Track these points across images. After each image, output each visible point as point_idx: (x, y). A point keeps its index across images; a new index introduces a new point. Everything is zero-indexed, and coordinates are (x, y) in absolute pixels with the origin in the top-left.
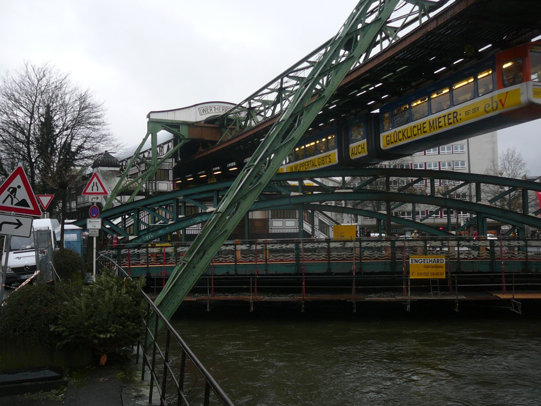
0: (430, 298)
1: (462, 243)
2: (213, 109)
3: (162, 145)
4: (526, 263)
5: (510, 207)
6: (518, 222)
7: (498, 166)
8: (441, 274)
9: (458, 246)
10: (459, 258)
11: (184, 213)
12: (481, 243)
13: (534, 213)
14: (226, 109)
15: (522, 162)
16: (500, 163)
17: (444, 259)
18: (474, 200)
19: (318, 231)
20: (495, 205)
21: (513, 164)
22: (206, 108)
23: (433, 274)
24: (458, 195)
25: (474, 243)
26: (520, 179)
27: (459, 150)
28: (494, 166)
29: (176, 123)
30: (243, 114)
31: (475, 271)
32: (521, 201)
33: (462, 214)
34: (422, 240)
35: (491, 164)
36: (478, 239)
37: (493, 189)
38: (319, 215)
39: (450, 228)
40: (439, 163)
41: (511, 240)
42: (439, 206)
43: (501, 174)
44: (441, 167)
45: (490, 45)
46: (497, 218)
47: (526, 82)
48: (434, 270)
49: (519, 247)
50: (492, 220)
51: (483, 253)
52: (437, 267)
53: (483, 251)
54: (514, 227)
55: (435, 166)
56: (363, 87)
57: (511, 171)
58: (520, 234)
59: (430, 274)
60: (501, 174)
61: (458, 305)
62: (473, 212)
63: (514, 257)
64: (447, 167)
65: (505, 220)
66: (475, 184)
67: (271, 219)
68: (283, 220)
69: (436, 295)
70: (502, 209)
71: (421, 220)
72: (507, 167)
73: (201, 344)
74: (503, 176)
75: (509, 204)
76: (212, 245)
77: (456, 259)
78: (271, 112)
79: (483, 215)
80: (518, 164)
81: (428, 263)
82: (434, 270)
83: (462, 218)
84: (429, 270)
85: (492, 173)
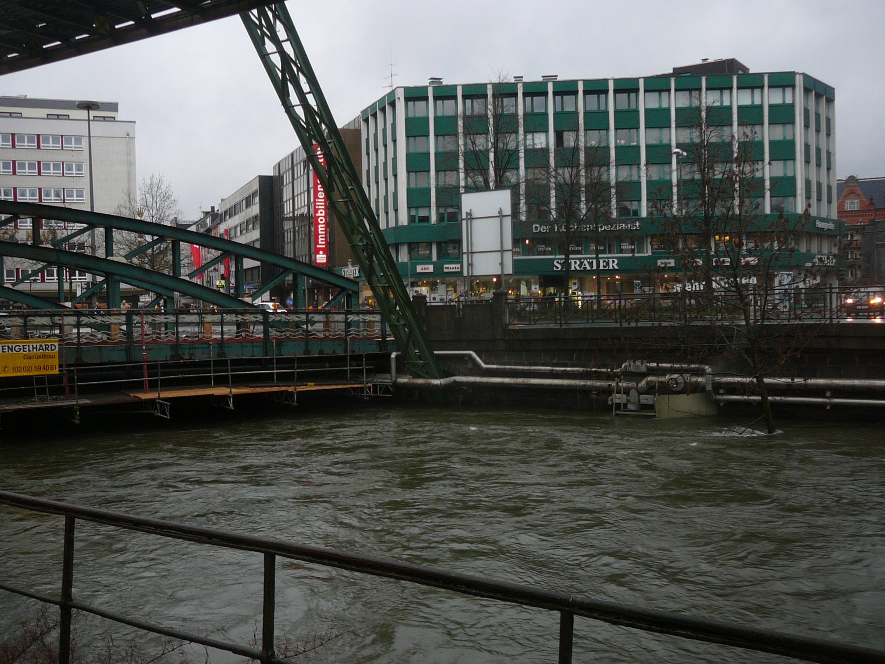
0: (35, 406)
1: (85, 320)
4: (177, 346)
5: (153, 267)
6: (166, 288)
7: (136, 201)
8: (52, 367)
9: (78, 325)
10: (79, 343)
12: (113, 320)
13: (188, 275)
15: (173, 198)
16: (138, 197)
17: (57, 344)
18: (101, 253)
20: (131, 262)
21: (158, 200)
23: (39, 368)
24: (73, 246)
25: (103, 319)
26: (168, 224)
27: (74, 171)
28: (130, 202)
31: (104, 360)
32: (171, 257)
33: (77, 277)
34: (20, 316)
35: (126, 198)
36: (109, 314)
37: (128, 238)
39: (62, 297)
40: (40, 189)
41: (155, 314)
42: (39, 260)
43: (140, 214)
44: (18, 197)
45: (132, 23)
46: (134, 282)
48: (40, 362)
49: (166, 325)
50: (131, 287)
51: (116, 334)
52: (44, 356)
53: (116, 331)
54: (159, 296)
55: (33, 195)
57: (155, 211)
58: (168, 306)
59: (33, 368)
60: (140, 214)
61: (78, 413)
62: (96, 272)
63: (160, 338)
64: (53, 197)
65: (148, 286)
66: (102, 230)
69: (42, 400)
70: (140, 268)
71: (14, 285)
72: (149, 204)
74: (143, 219)
75: (152, 262)
77: (73, 344)
79: (116, 277)
80: (165, 200)
81: (29, 351)
82: (40, 362)
83: (79, 283)
84: (33, 362)
85: (126, 214)
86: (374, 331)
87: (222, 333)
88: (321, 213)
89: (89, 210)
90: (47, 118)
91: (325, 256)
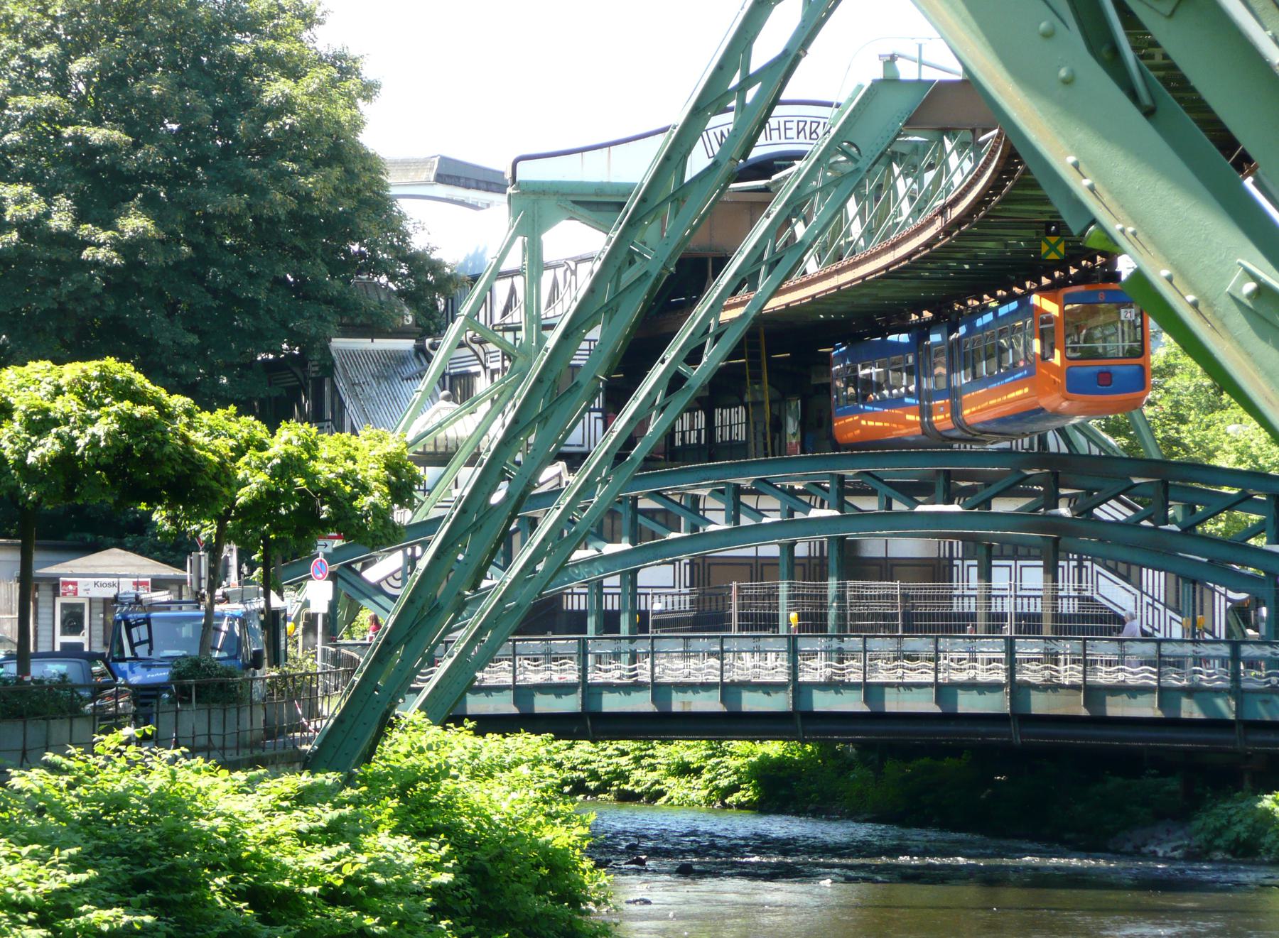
3: (572, 265)
14: (814, 125)
19: (1161, 608)
29: (610, 195)
47: (16, 640)
67: (963, 559)
68: (1012, 563)
78: (489, 432)
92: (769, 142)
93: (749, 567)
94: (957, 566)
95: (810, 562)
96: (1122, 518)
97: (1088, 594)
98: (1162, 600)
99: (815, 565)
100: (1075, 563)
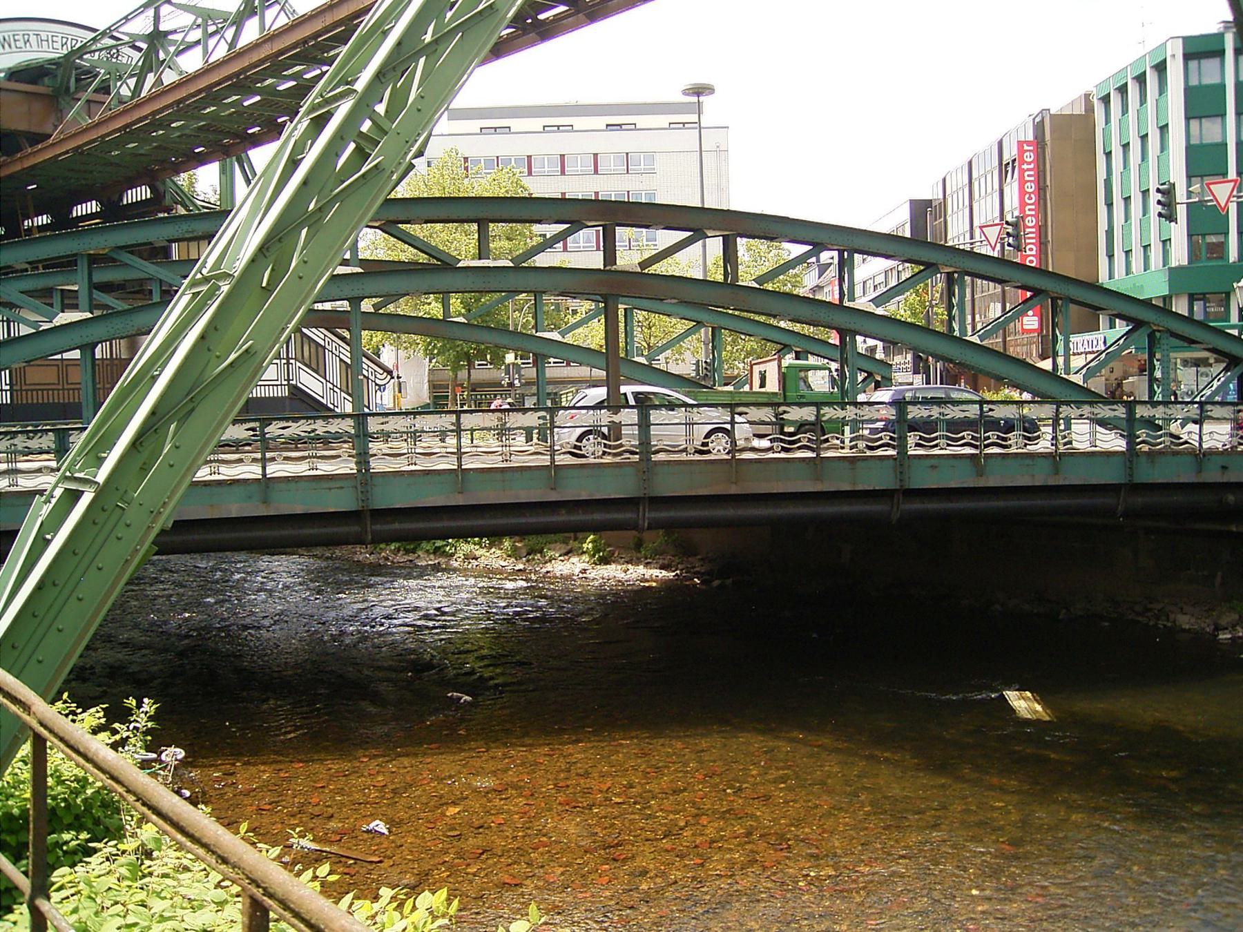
2: (33, 39)
11: (87, 307)
19: (338, 391)
22: (11, 34)
30: (131, 57)
38: (341, 350)
56: (290, 72)
73: (1157, 806)
76: (193, 410)
86: (621, 446)
87: (459, 454)
88: (1031, 250)
89: (700, 206)
90: (544, 131)
91: (1036, 318)
92: (40, 49)
93: (68, 367)
94: (99, 365)
95: (103, 363)
96: (313, 330)
97: (294, 382)
98: (339, 386)
99: (107, 365)
100: (284, 361)
